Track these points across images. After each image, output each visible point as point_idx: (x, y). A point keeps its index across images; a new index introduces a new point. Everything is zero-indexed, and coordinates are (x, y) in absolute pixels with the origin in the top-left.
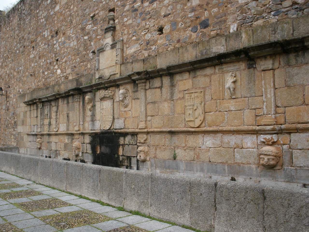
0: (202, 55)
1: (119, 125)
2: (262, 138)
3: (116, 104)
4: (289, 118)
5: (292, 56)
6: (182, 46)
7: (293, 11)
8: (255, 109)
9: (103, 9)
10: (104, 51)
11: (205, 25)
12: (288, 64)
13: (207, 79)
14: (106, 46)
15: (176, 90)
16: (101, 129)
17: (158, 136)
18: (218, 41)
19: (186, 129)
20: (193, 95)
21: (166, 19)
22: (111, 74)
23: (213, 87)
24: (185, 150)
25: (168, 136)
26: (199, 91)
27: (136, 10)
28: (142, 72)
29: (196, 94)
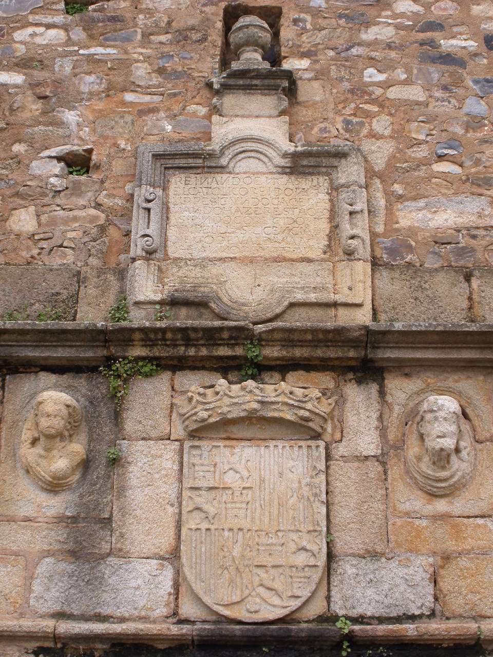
3: (347, 478)
10: (222, 169)
14: (238, 147)
16: (188, 609)
22: (300, 296)
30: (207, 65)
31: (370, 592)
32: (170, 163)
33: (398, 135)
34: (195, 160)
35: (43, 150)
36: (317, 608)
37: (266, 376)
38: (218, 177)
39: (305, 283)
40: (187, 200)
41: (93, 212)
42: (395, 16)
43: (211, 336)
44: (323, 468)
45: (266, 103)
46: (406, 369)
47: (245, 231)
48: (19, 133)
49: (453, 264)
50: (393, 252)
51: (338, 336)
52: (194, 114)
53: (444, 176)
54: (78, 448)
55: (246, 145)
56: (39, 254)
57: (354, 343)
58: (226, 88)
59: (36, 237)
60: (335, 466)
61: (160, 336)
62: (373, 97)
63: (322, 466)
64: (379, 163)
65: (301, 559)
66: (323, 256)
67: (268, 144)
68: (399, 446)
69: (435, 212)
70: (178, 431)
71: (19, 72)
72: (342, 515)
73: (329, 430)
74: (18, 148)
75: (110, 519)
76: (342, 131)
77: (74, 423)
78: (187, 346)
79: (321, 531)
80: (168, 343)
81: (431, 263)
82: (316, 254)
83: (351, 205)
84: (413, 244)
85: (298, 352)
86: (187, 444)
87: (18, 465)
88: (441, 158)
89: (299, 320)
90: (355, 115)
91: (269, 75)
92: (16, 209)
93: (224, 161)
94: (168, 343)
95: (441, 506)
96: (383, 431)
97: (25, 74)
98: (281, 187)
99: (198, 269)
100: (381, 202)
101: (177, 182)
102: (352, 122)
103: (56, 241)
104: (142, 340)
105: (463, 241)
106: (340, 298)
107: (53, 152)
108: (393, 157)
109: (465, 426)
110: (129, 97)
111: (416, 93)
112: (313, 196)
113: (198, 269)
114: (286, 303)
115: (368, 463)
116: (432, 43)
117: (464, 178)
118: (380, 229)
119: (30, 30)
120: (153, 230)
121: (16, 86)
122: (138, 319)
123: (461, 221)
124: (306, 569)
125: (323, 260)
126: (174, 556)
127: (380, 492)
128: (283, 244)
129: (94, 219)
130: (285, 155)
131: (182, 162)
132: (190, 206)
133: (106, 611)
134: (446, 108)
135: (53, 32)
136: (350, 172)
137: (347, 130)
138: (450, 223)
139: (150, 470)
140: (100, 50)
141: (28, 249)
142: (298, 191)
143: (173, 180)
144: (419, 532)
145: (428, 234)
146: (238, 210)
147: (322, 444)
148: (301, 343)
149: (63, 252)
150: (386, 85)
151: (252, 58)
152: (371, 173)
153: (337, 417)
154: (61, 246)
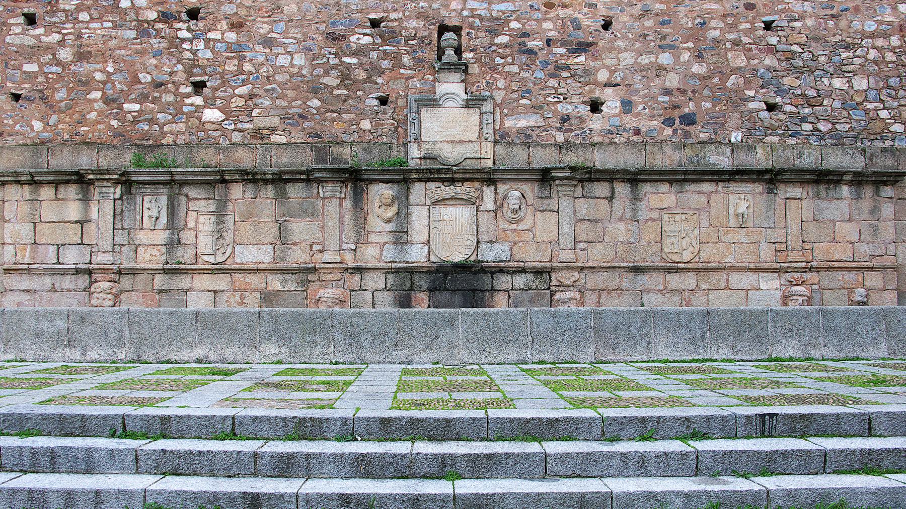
0: (691, 162)
1: (488, 255)
2: (789, 276)
3: (483, 217)
4: (818, 256)
5: (822, 187)
6: (644, 141)
7: (815, 138)
8: (774, 243)
9: (421, 15)
10: (440, 106)
11: (689, 120)
12: (817, 196)
13: (704, 199)
14: (446, 97)
15: (643, 205)
16: (433, 259)
17: (605, 274)
18: (720, 150)
19: (661, 264)
20: (677, 217)
21: (609, 91)
22: (468, 156)
23: (713, 210)
24: (663, 295)
25: (630, 275)
26: (691, 212)
27: (530, 52)
28: (579, 169)
29: (683, 217)
30: (430, 55)
31: (490, 253)
32: (421, 103)
34: (432, 102)
36: (473, 258)
37: (457, 184)
39: (469, 151)
42: (510, 30)
43: (439, 171)
45: (457, 76)
46: (503, 180)
50: (502, 137)
51: (481, 171)
54: (395, 209)
55: (449, 96)
57: (487, 173)
58: (441, 69)
65: (469, 243)
67: (457, 96)
68: (501, 207)
70: (428, 203)
72: (481, 229)
77: (394, 199)
81: (516, 141)
85: (467, 176)
88: (523, 97)
89: (468, 164)
91: (458, 64)
93: (441, 103)
95: (514, 226)
96: (496, 203)
100: (498, 117)
101: (424, 112)
105: (529, 132)
106: (482, 156)
107: (374, 95)
108: (504, 98)
109: (523, 201)
110: (402, 71)
111: (514, 69)
112: (473, 116)
116: (524, 44)
118: (498, 127)
119: (357, 36)
122: (412, 164)
126: (428, 242)
129: (393, 124)
131: (426, 103)
133: (407, 260)
134: (527, 75)
135: (366, 37)
136: (488, 107)
139: (419, 216)
140: (388, 48)
148: (470, 173)
150: (503, 65)
151: (450, 55)
152: (495, 105)
153: (480, 197)
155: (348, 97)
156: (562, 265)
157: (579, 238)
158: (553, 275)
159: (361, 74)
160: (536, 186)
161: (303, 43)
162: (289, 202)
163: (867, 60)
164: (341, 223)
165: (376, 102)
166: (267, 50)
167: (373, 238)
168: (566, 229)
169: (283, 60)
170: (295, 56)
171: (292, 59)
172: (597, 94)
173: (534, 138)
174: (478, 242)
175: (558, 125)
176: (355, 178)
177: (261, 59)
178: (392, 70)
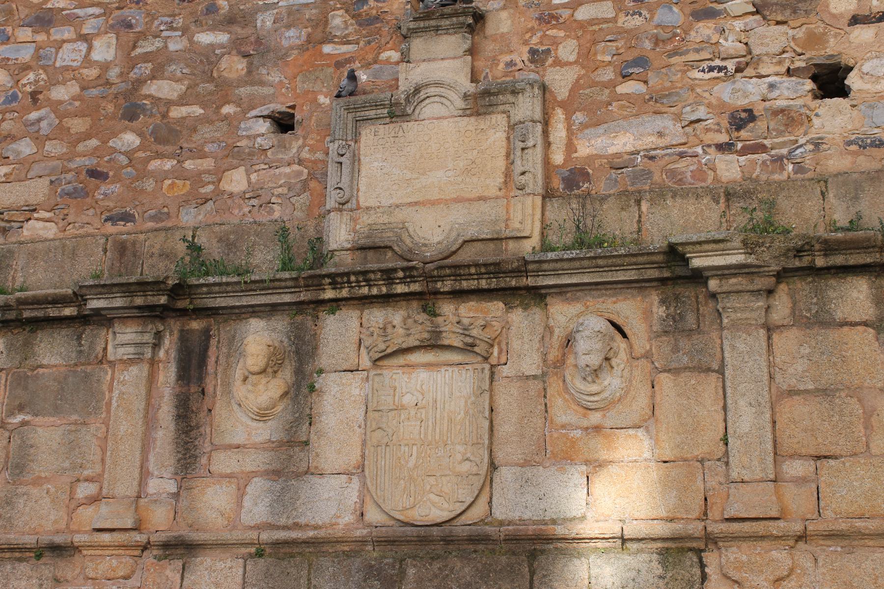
3: (508, 397)
33: (586, 57)
35: (250, 110)
36: (478, 512)
38: (405, 125)
40: (376, 151)
41: (296, 167)
43: (388, 275)
44: (487, 387)
47: (432, 173)
48: (227, 95)
49: (629, 188)
52: (387, 61)
53: (627, 96)
56: (250, 212)
59: (247, 196)
60: (499, 384)
61: (345, 279)
62: (561, 20)
63: (486, 386)
64: (562, 92)
65: (466, 467)
66: (499, 193)
67: (450, 87)
69: (615, 137)
70: (366, 362)
71: (224, 31)
72: (505, 429)
73: (496, 354)
74: (227, 109)
75: (307, 443)
76: (527, 63)
78: (370, 286)
79: (483, 444)
80: (353, 285)
82: (493, 192)
83: (523, 142)
84: (590, 171)
86: (372, 373)
87: (232, 401)
88: (626, 77)
90: (541, 43)
92: (228, 170)
94: (353, 285)
97: (229, 33)
98: (461, 129)
99: (385, 216)
102: (538, 51)
103: (264, 199)
104: (330, 284)
110: (327, 49)
112: (494, 132)
113: (385, 216)
114: (460, 241)
115: (530, 382)
117: (647, 97)
120: (345, 182)
121: (222, 46)
123: (640, 145)
124: (470, 477)
125: (497, 198)
127: (539, 407)
128: (462, 186)
129: (300, 173)
130: (466, 97)
132: (379, 156)
136: (527, 107)
137: (532, 61)
138: (629, 148)
139: (341, 399)
141: (240, 207)
142: (478, 131)
143: (363, 133)
144: (574, 442)
145: (606, 161)
146: (422, 156)
147: (487, 366)
148: (528, 289)
149: (272, 209)
154: (269, 203)
155: (204, 120)
156: (735, 527)
157: (788, 444)
158: (710, 558)
159: (233, 67)
160: (655, 306)
161: (117, 13)
162: (37, 377)
163: (587, 71)
164: (150, 422)
165: (264, 126)
166: (41, 37)
167: (223, 463)
168: (747, 419)
169: (70, 55)
170: (97, 43)
171: (90, 48)
172: (833, 48)
173: (656, 177)
174: (493, 467)
175: (723, 138)
176: (182, 307)
177: (26, 55)
178: (303, 49)
